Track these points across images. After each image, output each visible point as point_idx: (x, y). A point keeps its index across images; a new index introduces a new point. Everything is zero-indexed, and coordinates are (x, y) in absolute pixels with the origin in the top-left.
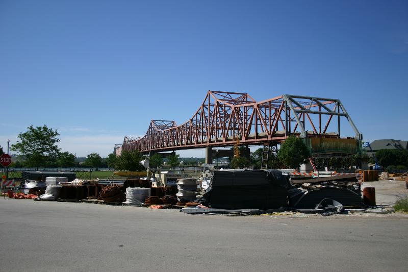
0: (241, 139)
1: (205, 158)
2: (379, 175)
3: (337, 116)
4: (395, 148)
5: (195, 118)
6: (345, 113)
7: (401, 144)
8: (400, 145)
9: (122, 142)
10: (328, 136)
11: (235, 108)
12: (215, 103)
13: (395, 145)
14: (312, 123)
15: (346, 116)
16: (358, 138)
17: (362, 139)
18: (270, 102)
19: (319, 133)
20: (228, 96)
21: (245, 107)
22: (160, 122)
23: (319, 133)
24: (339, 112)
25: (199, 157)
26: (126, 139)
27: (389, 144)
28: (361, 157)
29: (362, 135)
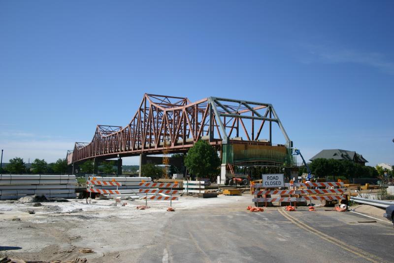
0: (170, 145)
1: (139, 166)
2: (170, 171)
3: (269, 122)
4: (341, 158)
5: (133, 123)
6: (276, 118)
7: (349, 154)
8: (347, 156)
9: (72, 148)
10: (262, 144)
11: (167, 112)
12: (150, 106)
13: (342, 156)
14: (246, 132)
15: (277, 121)
16: (288, 145)
17: (292, 146)
18: (197, 105)
19: (251, 140)
20: (166, 100)
21: (175, 111)
22: (107, 128)
23: (251, 140)
24: (271, 117)
25: (130, 165)
26: (77, 145)
27: (335, 155)
28: (290, 166)
29: (292, 142)
